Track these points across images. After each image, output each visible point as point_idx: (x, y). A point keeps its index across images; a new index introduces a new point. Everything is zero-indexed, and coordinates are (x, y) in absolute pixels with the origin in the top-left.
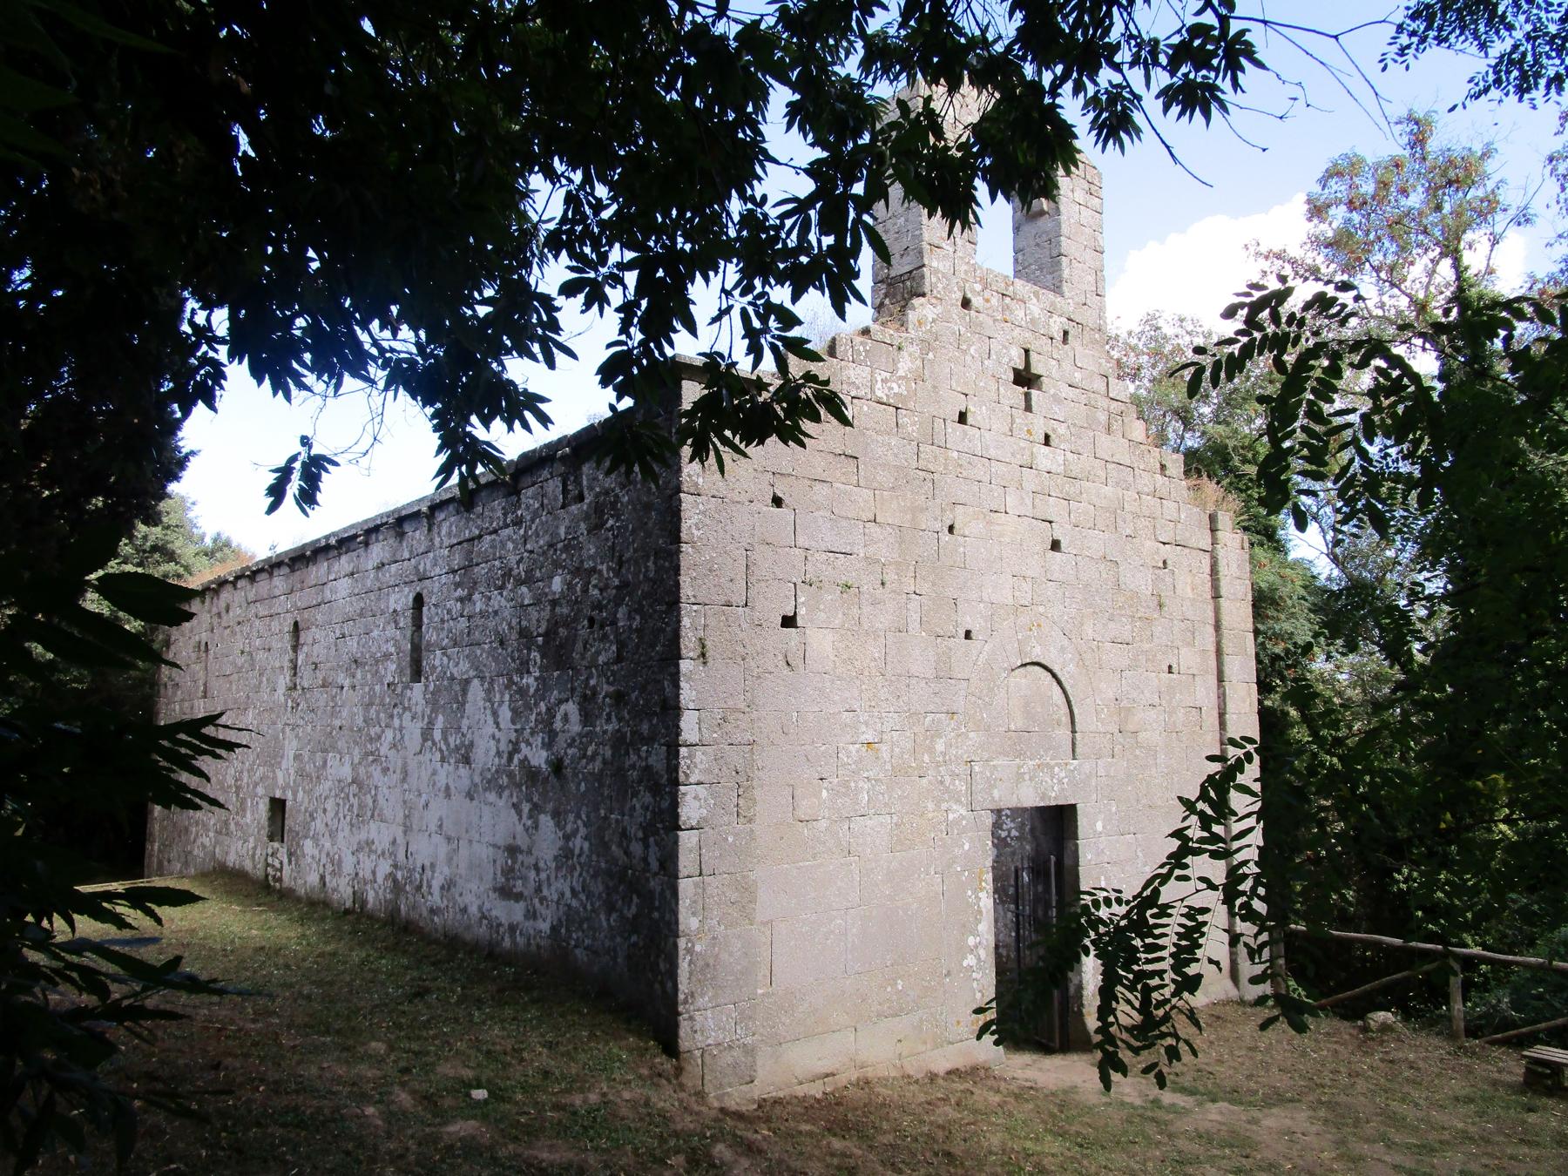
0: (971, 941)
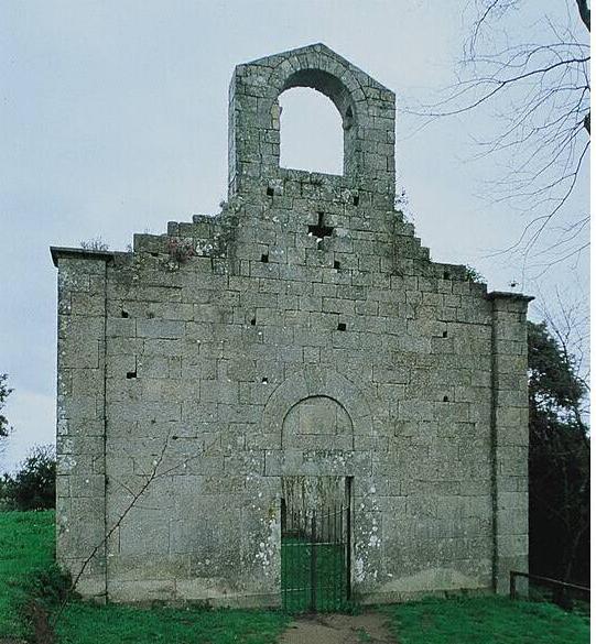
0: (262, 545)
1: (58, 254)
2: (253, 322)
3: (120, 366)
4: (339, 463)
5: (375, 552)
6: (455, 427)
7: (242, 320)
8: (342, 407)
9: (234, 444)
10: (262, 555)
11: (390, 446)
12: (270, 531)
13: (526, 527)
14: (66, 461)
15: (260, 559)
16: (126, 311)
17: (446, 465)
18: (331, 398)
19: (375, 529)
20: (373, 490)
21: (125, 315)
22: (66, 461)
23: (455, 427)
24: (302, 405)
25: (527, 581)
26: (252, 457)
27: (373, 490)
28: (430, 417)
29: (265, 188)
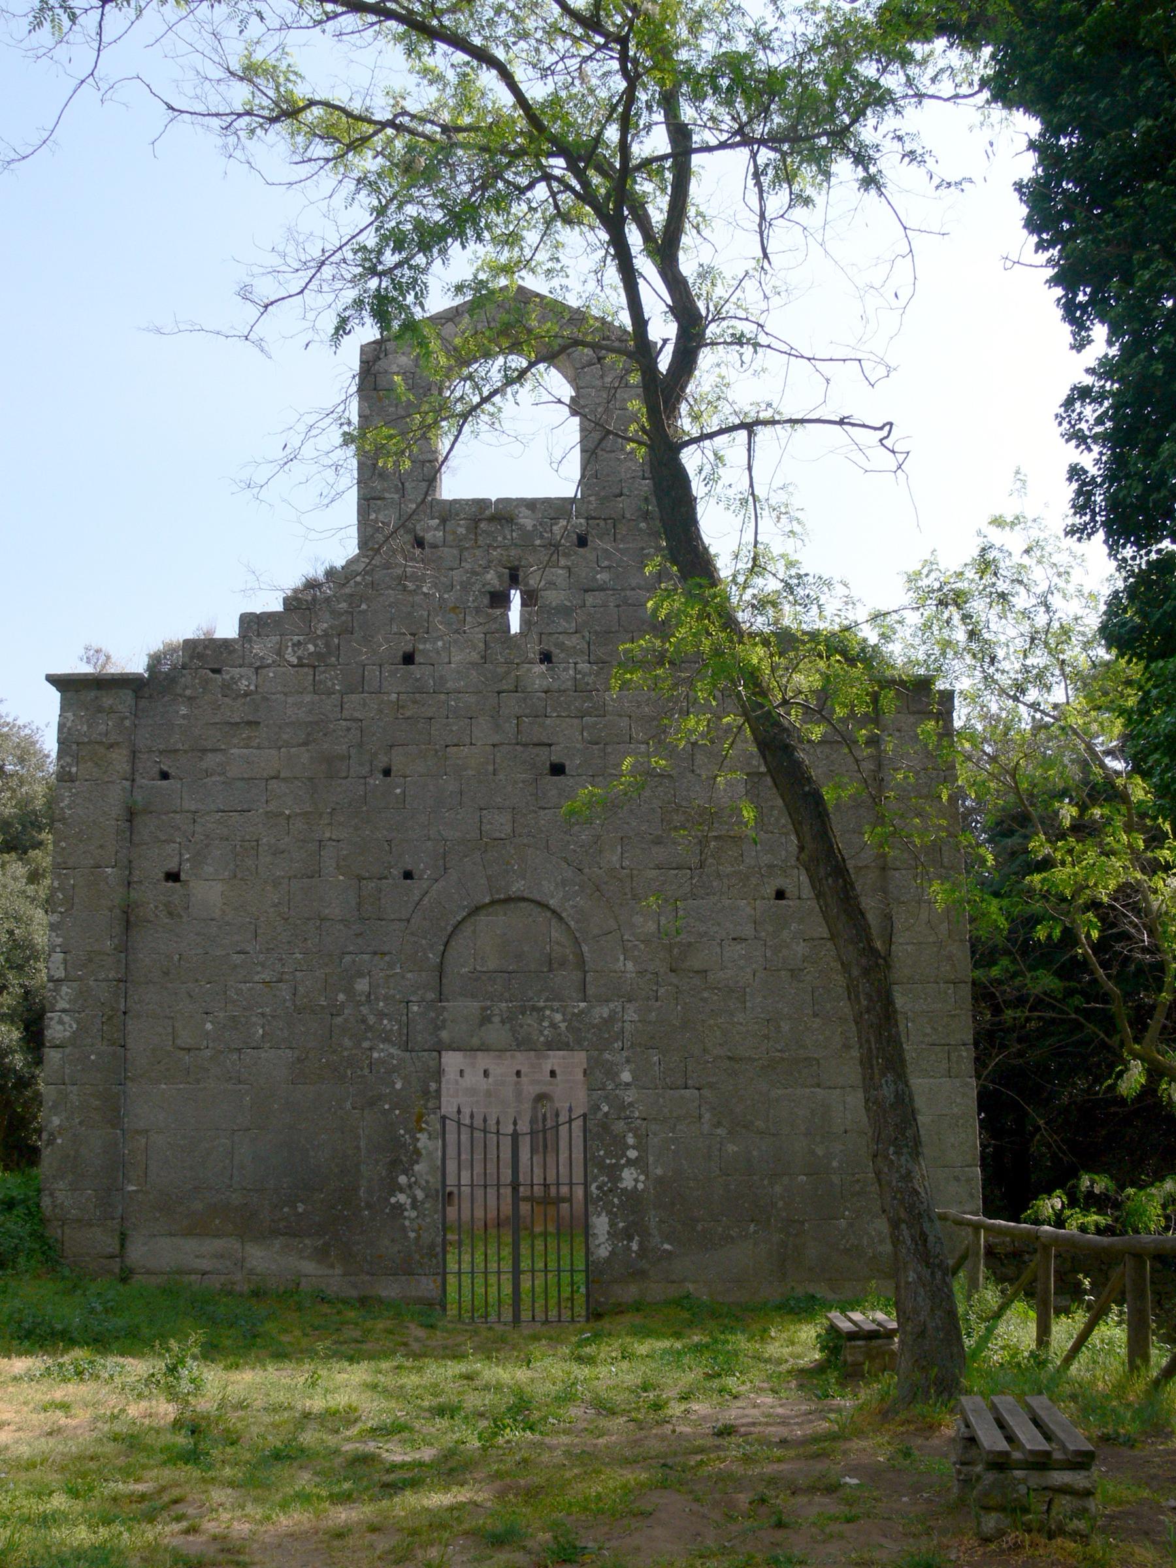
0: (403, 1179)
1: (54, 680)
2: (387, 772)
3: (153, 864)
4: (553, 1025)
5: (632, 1198)
6: (801, 949)
7: (364, 771)
8: (560, 918)
9: (350, 991)
10: (402, 1198)
11: (662, 991)
12: (417, 1152)
13: (700, 509)
14: (61, 1022)
15: (400, 1207)
16: (165, 768)
17: (785, 1026)
18: (539, 903)
19: (632, 1154)
20: (626, 1076)
21: (165, 776)
22: (61, 1022)
23: (801, 949)
24: (482, 919)
25: (510, 357)
26: (381, 1015)
27: (626, 1076)
28: (748, 930)
29: (409, 538)
